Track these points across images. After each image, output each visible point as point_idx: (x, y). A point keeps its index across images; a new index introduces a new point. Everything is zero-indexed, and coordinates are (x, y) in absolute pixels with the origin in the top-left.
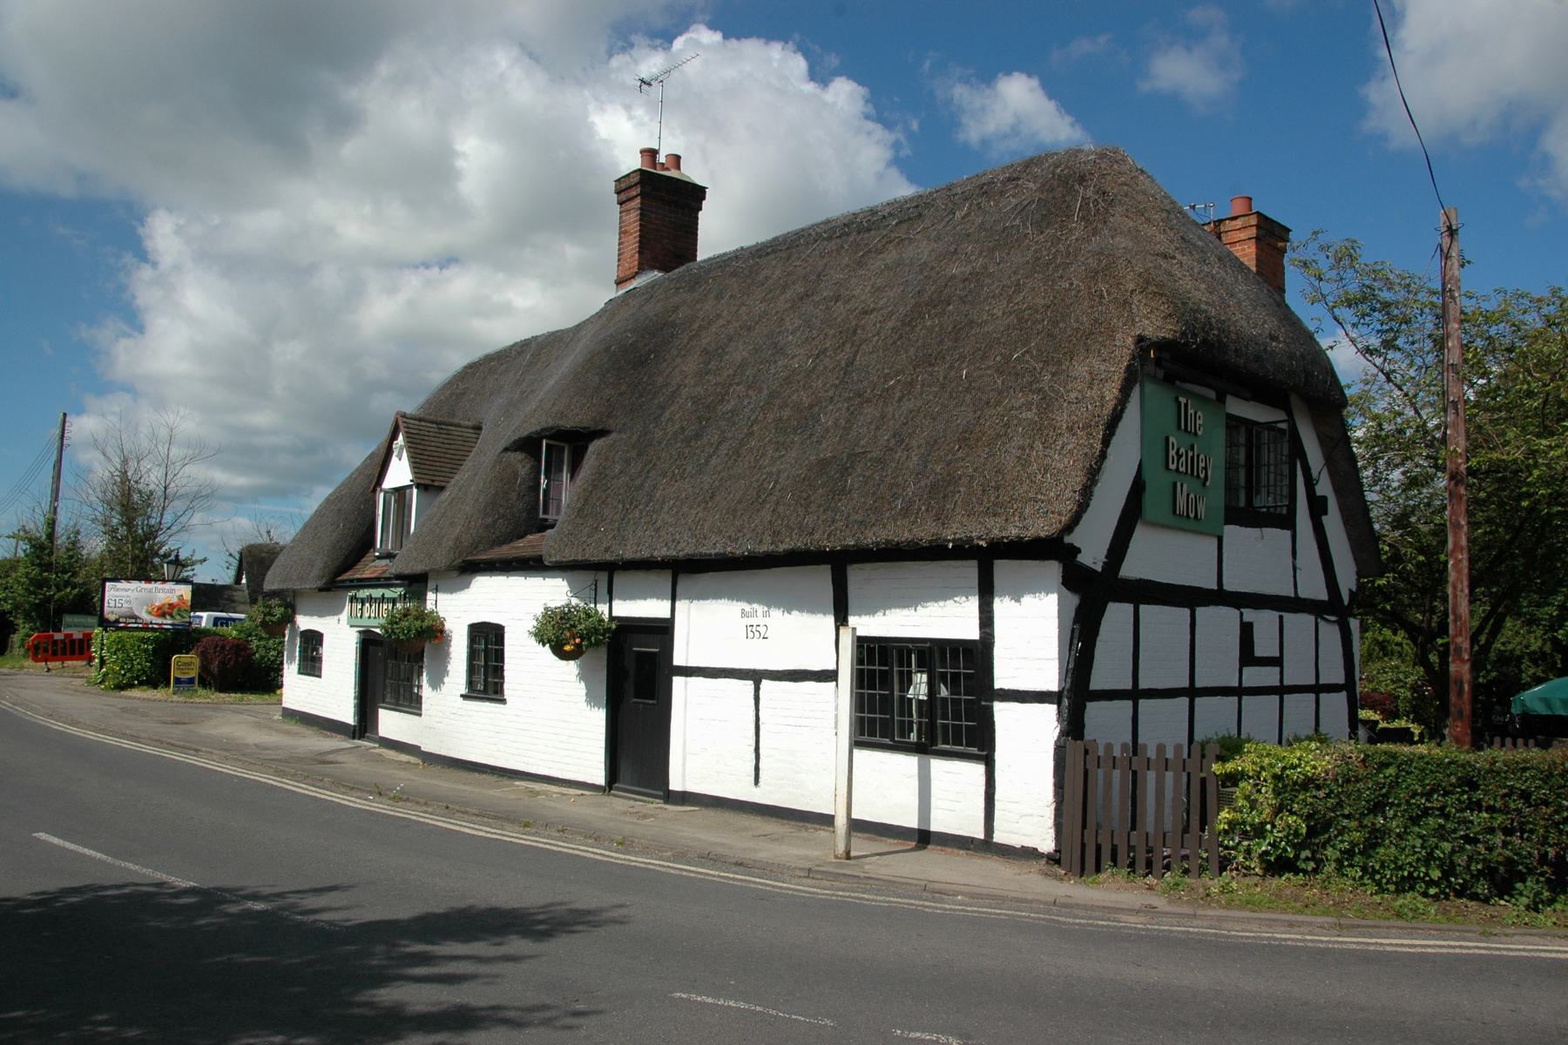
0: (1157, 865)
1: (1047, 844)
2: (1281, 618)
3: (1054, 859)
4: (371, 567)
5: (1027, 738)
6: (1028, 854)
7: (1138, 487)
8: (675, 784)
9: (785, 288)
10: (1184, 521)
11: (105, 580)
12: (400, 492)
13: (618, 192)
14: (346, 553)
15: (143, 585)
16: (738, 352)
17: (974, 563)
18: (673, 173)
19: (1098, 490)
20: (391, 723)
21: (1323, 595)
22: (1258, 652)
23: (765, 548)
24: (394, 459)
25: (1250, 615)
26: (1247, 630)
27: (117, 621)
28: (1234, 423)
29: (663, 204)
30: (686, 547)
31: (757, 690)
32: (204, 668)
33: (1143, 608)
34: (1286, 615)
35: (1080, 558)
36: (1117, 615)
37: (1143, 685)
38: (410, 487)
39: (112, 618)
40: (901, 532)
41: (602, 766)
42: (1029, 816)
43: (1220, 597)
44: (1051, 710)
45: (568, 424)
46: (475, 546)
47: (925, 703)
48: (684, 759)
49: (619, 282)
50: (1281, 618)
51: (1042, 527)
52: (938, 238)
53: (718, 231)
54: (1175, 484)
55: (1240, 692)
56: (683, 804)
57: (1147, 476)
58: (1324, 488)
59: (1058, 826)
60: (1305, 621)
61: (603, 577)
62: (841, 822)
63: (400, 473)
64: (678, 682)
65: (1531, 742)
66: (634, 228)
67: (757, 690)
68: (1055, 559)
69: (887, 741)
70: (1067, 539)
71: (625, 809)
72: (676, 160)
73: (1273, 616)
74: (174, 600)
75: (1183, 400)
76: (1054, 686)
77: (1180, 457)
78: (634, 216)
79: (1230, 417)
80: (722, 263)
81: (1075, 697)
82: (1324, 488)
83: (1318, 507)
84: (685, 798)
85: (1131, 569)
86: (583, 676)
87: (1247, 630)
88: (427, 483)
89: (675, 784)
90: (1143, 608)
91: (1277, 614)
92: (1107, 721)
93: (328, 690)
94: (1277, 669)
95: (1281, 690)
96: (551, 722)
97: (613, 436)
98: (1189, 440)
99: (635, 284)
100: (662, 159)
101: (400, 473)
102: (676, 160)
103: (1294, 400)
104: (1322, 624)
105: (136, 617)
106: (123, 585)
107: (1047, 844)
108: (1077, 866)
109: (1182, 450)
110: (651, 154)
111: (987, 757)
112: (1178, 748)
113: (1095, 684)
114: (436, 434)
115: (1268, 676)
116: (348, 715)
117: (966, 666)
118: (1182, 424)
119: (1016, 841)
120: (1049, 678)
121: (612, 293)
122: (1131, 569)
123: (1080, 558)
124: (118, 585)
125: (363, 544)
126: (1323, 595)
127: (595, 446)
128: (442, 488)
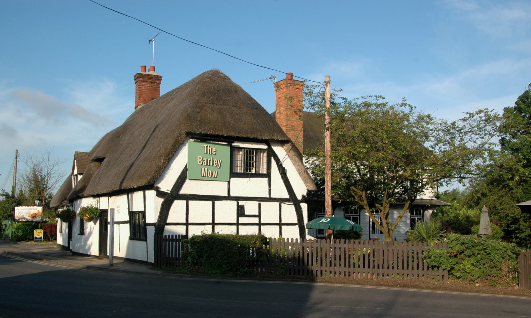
2: (260, 204)
11: (15, 207)
15: (27, 207)
22: (258, 214)
25: (241, 203)
27: (19, 220)
29: (148, 82)
32: (45, 234)
33: (190, 202)
36: (178, 206)
37: (258, 227)
39: (17, 218)
43: (229, 198)
50: (260, 204)
53: (165, 89)
65: (286, 241)
72: (154, 69)
73: (256, 203)
74: (36, 212)
83: (283, 172)
90: (190, 202)
102: (154, 69)
105: (25, 218)
106: (20, 208)
111: (146, 240)
112: (297, 239)
113: (169, 221)
124: (19, 208)
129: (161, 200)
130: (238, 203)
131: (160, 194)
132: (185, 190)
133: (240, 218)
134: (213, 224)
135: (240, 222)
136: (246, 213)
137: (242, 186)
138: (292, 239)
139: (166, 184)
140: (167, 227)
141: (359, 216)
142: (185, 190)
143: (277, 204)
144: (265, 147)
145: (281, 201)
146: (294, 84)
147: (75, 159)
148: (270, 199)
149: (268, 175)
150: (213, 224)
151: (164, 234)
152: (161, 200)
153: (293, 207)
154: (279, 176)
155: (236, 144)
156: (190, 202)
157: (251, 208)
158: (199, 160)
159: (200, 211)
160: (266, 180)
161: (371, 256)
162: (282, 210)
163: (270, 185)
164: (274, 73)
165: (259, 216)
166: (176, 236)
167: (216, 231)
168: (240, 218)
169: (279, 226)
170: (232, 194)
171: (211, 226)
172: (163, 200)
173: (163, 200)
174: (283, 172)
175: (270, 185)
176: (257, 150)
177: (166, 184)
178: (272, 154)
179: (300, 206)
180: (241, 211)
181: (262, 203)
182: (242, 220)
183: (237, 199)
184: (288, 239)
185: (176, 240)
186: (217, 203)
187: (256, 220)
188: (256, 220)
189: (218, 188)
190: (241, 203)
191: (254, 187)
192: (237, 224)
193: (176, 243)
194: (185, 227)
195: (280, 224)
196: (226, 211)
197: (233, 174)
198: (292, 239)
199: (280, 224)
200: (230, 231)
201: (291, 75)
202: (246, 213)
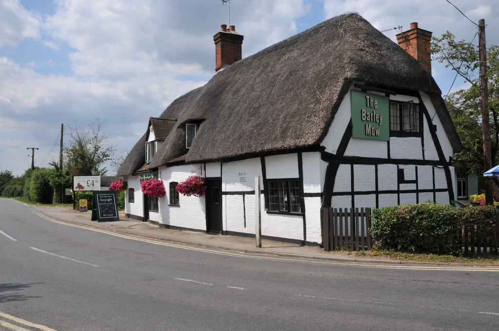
0: (357, 248)
1: (320, 241)
2: (416, 167)
3: (321, 246)
4: (145, 167)
5: (313, 206)
6: (315, 244)
7: (350, 127)
8: (224, 229)
9: (258, 68)
10: (371, 136)
12: (153, 142)
13: (215, 40)
14: (138, 163)
16: (243, 91)
17: (297, 154)
18: (233, 32)
19: (331, 130)
20: (153, 216)
21: (437, 159)
22: (406, 179)
23: (240, 153)
24: (151, 132)
25: (401, 166)
26: (401, 173)
28: (392, 103)
29: (229, 43)
30: (223, 154)
31: (244, 197)
33: (355, 166)
34: (418, 166)
35: (326, 150)
36: (343, 170)
38: (155, 141)
40: (279, 145)
41: (205, 224)
42: (315, 234)
43: (389, 161)
44: (319, 198)
45: (193, 118)
46: (170, 158)
47: (283, 197)
48: (226, 221)
49: (217, 70)
50: (416, 167)
51: (311, 141)
52: (300, 49)
53: (248, 51)
54: (366, 125)
55: (398, 192)
56: (227, 235)
57: (353, 123)
58: (436, 121)
59: (322, 235)
60: (429, 168)
61: (203, 165)
62: (258, 236)
63: (152, 137)
64: (224, 196)
66: (220, 51)
67: (244, 197)
68: (320, 152)
69: (278, 212)
70: (321, 145)
71: (208, 239)
73: (413, 166)
75: (368, 97)
76: (320, 191)
77: (367, 115)
78: (219, 48)
79: (390, 101)
80: (247, 59)
81: (327, 195)
82: (436, 121)
83: (433, 129)
84: (227, 233)
85: (349, 152)
86: (201, 200)
87: (401, 173)
88: (160, 139)
89: (224, 229)
90: (355, 166)
91: (414, 166)
92: (340, 203)
93: (137, 207)
94: (415, 184)
95: (417, 191)
96: (191, 211)
97: (206, 121)
98: (372, 110)
99: (221, 70)
100: (228, 27)
101: (152, 137)
102: (233, 28)
103: (421, 93)
104: (435, 168)
107: (320, 241)
108: (328, 248)
109: (368, 113)
110: (224, 27)
111: (303, 215)
113: (336, 190)
114: (160, 125)
115: (412, 187)
116: (142, 215)
117: (295, 186)
118: (369, 105)
119: (312, 241)
120: (319, 189)
121: (215, 73)
122: (349, 152)
123: (326, 150)
125: (142, 162)
126: (437, 159)
127: (202, 125)
128: (164, 140)
130: (398, 167)
131: (326, 157)
135: (401, 189)
138: (341, 209)
139: (331, 145)
140: (334, 198)
141: (467, 179)
144: (416, 101)
145: (434, 163)
147: (150, 125)
149: (420, 134)
153: (444, 173)
154: (430, 135)
155: (393, 98)
157: (409, 171)
158: (363, 115)
159: (364, 175)
162: (435, 173)
163: (33, 163)
165: (416, 182)
166: (362, 209)
170: (393, 157)
171: (355, 196)
174: (433, 129)
175: (33, 163)
180: (401, 178)
182: (403, 187)
183: (397, 162)
186: (380, 166)
187: (412, 187)
189: (377, 150)
195: (377, 192)
196: (388, 175)
198: (341, 209)
199: (353, 193)
201: (416, 24)
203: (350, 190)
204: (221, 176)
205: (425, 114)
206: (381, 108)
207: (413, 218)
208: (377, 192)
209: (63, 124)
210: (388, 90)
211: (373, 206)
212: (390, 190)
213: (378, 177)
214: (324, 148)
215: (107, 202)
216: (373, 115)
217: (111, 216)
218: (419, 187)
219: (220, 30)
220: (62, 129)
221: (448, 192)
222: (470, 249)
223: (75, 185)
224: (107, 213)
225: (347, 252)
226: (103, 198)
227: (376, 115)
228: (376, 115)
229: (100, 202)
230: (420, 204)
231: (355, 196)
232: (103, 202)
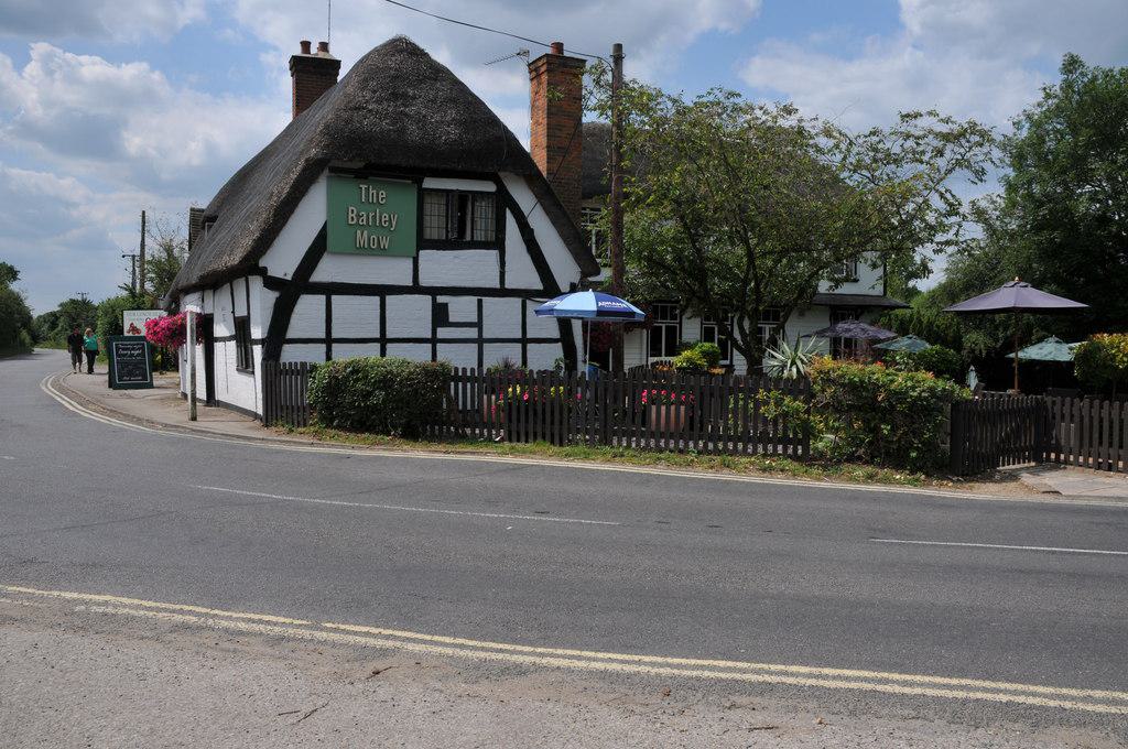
2: (480, 302)
21: (539, 286)
25: (441, 299)
33: (333, 297)
35: (269, 274)
43: (416, 288)
50: (480, 302)
73: (474, 299)
84: (227, 406)
91: (476, 298)
92: (291, 354)
102: (324, 46)
112: (473, 370)
113: (291, 334)
126: (539, 286)
129: (272, 296)
130: (434, 300)
131: (271, 283)
132: (326, 272)
133: (439, 330)
134: (329, 341)
136: (451, 320)
137: (441, 267)
138: (464, 370)
139: (283, 260)
140: (286, 347)
141: (680, 324)
142: (326, 272)
143: (517, 302)
144: (490, 187)
145: (526, 295)
146: (565, 66)
148: (502, 292)
149: (498, 244)
150: (383, 340)
151: (282, 361)
152: (272, 296)
155: (430, 183)
156: (334, 298)
157: (461, 308)
159: (356, 315)
160: (494, 254)
161: (697, 406)
164: (526, 46)
165: (479, 325)
167: (440, 358)
168: (439, 330)
169: (430, 336)
172: (277, 294)
173: (277, 294)
176: (474, 193)
177: (283, 260)
178: (504, 201)
179: (519, 296)
180: (440, 316)
181: (487, 300)
182: (442, 333)
183: (433, 291)
184: (456, 369)
185: (456, 379)
186: (390, 299)
187: (472, 333)
188: (472, 333)
189: (395, 271)
190: (441, 299)
191: (473, 267)
192: (434, 341)
193: (473, 388)
194: (323, 347)
196: (411, 315)
197: (424, 243)
198: (464, 370)
200: (420, 355)
201: (559, 47)
202: (451, 320)
203: (519, 336)
204: (249, 313)
205: (512, 212)
206: (393, 205)
207: (346, 378)
208: (524, 341)
209: (144, 212)
210: (414, 174)
211: (517, 361)
212: (414, 337)
213: (387, 316)
214: (265, 270)
215: (132, 355)
216: (374, 217)
217: (138, 380)
218: (333, 331)
219: (298, 51)
220: (144, 222)
221: (560, 344)
222: (477, 431)
223: (127, 327)
224: (130, 374)
225: (286, 429)
226: (123, 349)
227: (381, 217)
228: (381, 217)
229: (118, 355)
230: (387, 357)
231: (324, 345)
232: (125, 355)
